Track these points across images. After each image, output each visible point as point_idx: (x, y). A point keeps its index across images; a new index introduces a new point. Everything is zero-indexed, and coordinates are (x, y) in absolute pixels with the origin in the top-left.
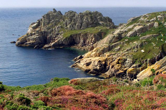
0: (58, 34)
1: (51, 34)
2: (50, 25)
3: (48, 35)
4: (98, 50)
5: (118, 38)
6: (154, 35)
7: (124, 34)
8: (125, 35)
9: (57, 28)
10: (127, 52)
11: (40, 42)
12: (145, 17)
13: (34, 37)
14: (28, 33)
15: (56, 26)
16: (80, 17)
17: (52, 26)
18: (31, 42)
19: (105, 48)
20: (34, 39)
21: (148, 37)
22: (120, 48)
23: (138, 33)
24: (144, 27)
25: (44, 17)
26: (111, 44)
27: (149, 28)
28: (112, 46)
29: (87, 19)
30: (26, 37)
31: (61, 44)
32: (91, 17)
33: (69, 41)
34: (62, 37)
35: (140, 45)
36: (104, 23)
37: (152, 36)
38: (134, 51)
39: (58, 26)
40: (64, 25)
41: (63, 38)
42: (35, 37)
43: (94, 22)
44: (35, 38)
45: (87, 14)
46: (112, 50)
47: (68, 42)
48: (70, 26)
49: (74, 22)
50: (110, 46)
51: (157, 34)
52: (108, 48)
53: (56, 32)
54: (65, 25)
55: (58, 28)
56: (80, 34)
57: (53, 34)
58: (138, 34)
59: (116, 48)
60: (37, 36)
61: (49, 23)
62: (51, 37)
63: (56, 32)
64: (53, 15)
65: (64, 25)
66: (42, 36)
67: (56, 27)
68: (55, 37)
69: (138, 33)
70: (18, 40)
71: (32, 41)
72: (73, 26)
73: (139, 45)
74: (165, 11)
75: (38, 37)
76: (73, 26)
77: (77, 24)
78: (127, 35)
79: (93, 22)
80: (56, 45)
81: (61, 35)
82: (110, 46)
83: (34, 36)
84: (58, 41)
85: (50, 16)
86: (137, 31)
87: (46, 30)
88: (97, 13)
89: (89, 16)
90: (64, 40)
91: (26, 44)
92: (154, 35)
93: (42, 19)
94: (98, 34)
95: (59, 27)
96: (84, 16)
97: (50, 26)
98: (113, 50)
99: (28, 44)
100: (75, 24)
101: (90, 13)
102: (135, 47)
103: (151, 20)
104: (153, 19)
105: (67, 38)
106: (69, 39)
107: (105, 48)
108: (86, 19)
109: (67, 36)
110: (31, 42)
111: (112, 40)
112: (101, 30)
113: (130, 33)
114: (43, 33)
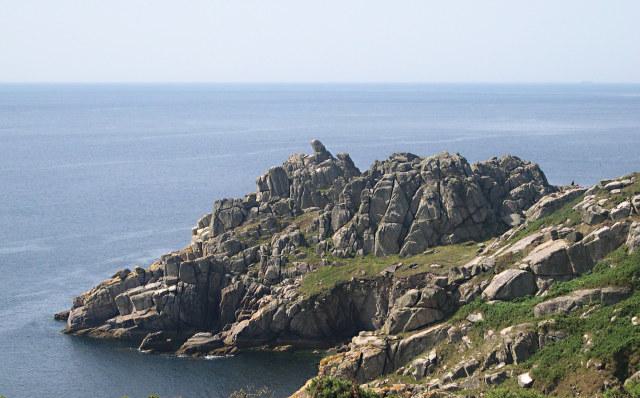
0: (277, 279)
1: (247, 277)
2: (245, 230)
3: (230, 279)
4: (330, 367)
5: (439, 308)
6: (605, 290)
7: (471, 287)
8: (476, 288)
9: (276, 245)
10: (454, 385)
11: (182, 315)
12: (604, 189)
13: (156, 288)
14: (128, 272)
15: (276, 235)
16: (401, 186)
17: (258, 235)
18: (136, 314)
19: (365, 356)
20: (147, 302)
21: (574, 304)
22: (435, 360)
23: (543, 282)
24: (574, 250)
25: (262, 184)
26: (400, 338)
27: (598, 251)
28: (405, 348)
29: (436, 198)
30: (112, 291)
31: (281, 331)
32: (459, 191)
33: (324, 318)
34: (289, 294)
35: (520, 344)
37: (596, 296)
38: (488, 380)
39: (283, 237)
40: (315, 229)
41: (294, 299)
42: (156, 292)
43: (475, 217)
44: (158, 297)
45: (438, 174)
46: (402, 372)
48: (346, 237)
49: (365, 217)
50: (393, 347)
51: (624, 290)
52: (381, 359)
53: (270, 268)
54: (322, 230)
55: (282, 244)
57: (256, 275)
58: (540, 282)
59: (420, 360)
60: (170, 283)
62: (242, 289)
63: (270, 268)
64: (308, 176)
65: (315, 229)
66: (192, 286)
67: (277, 238)
68: (260, 295)
69: (543, 282)
70: (78, 304)
71: (139, 313)
72: (359, 237)
73: (517, 341)
75: (175, 292)
76: (359, 237)
77: (381, 226)
78: (488, 288)
79: (470, 216)
80: (256, 336)
81: (292, 282)
82: (393, 347)
83: (153, 285)
84: (268, 315)
85: (291, 182)
86: (535, 269)
87: (221, 256)
88: (513, 162)
89: (445, 183)
90: (298, 307)
91: (114, 325)
92: (606, 294)
95: (287, 239)
96: (421, 181)
97: (248, 235)
98: (406, 371)
99: (120, 325)
100: (372, 225)
101: (459, 167)
102: (499, 356)
103: (614, 211)
104: (624, 204)
105: (314, 298)
106: (323, 305)
107: (365, 356)
108: (429, 200)
109: (315, 289)
110: (134, 318)
111: (408, 314)
113: (504, 277)
114: (204, 270)
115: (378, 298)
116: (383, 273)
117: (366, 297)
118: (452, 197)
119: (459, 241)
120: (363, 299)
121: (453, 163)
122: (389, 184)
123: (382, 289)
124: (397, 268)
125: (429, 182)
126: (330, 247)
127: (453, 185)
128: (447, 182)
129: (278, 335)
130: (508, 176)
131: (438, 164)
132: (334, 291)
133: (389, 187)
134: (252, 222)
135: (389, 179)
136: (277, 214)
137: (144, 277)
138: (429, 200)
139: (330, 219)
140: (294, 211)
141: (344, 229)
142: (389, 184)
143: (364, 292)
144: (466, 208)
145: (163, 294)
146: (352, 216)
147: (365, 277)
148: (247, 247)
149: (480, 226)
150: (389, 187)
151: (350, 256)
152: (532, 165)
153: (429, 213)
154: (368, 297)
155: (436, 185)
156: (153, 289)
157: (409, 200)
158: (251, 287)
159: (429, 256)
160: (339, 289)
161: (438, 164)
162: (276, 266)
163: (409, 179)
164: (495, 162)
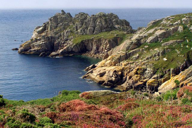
0: (67, 40)
1: (59, 40)
2: (58, 29)
3: (56, 40)
4: (113, 58)
5: (137, 45)
6: (178, 40)
7: (144, 40)
8: (145, 41)
9: (65, 32)
10: (147, 61)
11: (46, 49)
12: (168, 19)
13: (40, 43)
14: (33, 39)
15: (64, 31)
16: (93, 19)
17: (61, 31)
18: (36, 48)
19: (121, 55)
20: (39, 45)
21: (171, 43)
22: (138, 56)
23: (160, 39)
24: (167, 32)
25: (51, 20)
26: (129, 52)
27: (172, 32)
28: (130, 54)
29: (101, 22)
30: (30, 44)
31: (70, 51)
32: (106, 20)
33: (79, 48)
34: (71, 43)
35: (162, 52)
36: (120, 27)
37: (176, 42)
38: (156, 60)
39: (67, 31)
40: (74, 29)
41: (73, 44)
42: (40, 43)
43: (109, 26)
44: (41, 44)
45: (100, 17)
46: (130, 59)
47: (78, 49)
48: (81, 31)
49: (85, 26)
50: (128, 53)
51: (182, 40)
52: (125, 56)
53: (65, 38)
54: (75, 29)
55: (67, 32)
56: (92, 40)
57: (61, 39)
58: (159, 39)
59: (134, 56)
60: (43, 41)
61: (57, 27)
62: (59, 43)
63: (65, 38)
64: (62, 18)
65: (74, 29)
66: (48, 42)
67: (65, 31)
68: (64, 43)
69: (160, 39)
70: (21, 46)
71: (37, 48)
72: (84, 31)
73: (161, 52)
74: (191, 13)
75: (44, 43)
76: (84, 31)
77: (89, 28)
78: (147, 41)
79: (108, 26)
80: (65, 53)
81: (70, 41)
82: (128, 53)
83: (39, 42)
84: (68, 48)
85: (58, 19)
86: (158, 36)
87: (53, 35)
88: (112, 15)
89: (102, 19)
90: (74, 46)
91: (31, 51)
92: (179, 41)
93: (48, 22)
94: (113, 40)
95: (68, 31)
96: (97, 18)
97: (58, 30)
98: (131, 59)
99: (32, 51)
100: (87, 28)
101: (104, 15)
102: (156, 55)
103: (174, 24)
104: (177, 22)
105: (77, 44)
106: (79, 45)
107: (121, 55)
108: (99, 22)
109: (77, 42)
110: (36, 49)
111: (130, 46)
112: (117, 35)
113: (151, 38)
114: (50, 38)
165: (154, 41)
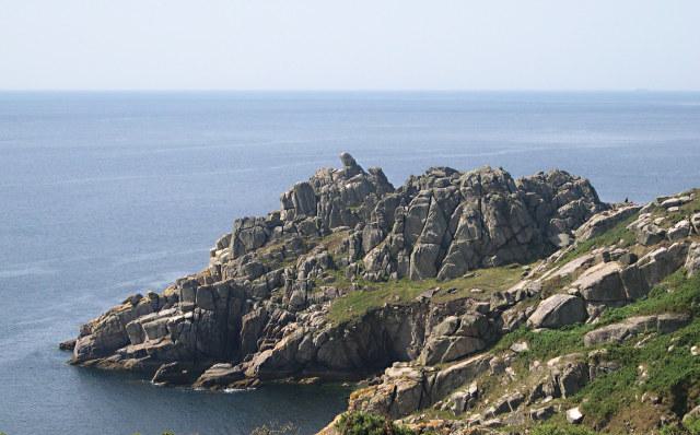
0: (303, 305)
1: (270, 303)
2: (268, 251)
3: (251, 305)
4: (361, 401)
5: (480, 337)
6: (662, 317)
7: (516, 314)
8: (521, 315)
9: (302, 268)
10: (496, 420)
11: (199, 344)
12: (660, 207)
13: (170, 315)
14: (140, 297)
15: (302, 257)
16: (439, 203)
17: (282, 256)
18: (149, 344)
19: (400, 389)
20: (161, 331)
21: (628, 332)
22: (475, 394)
23: (594, 308)
24: (628, 273)
25: (286, 201)
26: (437, 370)
27: (654, 275)
28: (442, 380)
29: (477, 216)
30: (123, 318)
31: (307, 362)
32: (502, 208)
33: (354, 347)
34: (316, 322)
35: (568, 376)
37: (652, 323)
38: (534, 415)
39: (309, 259)
40: (344, 250)
41: (321, 327)
42: (171, 320)
43: (520, 238)
44: (173, 324)
45: (479, 190)
46: (440, 406)
48: (379, 259)
49: (399, 237)
50: (430, 379)
51: (683, 317)
52: (417, 393)
53: (295, 293)
54: (352, 251)
55: (308, 267)
57: (280, 301)
58: (591, 308)
59: (459, 394)
60: (185, 310)
62: (265, 316)
63: (295, 293)
64: (336, 192)
65: (344, 250)
66: (210, 313)
67: (303, 260)
68: (285, 322)
69: (594, 308)
70: (85, 332)
71: (152, 342)
72: (392, 259)
73: (566, 373)
75: (191, 319)
76: (392, 259)
77: (417, 247)
78: (534, 315)
79: (514, 236)
80: (280, 367)
81: (319, 308)
82: (430, 379)
83: (167, 312)
84: (293, 344)
85: (318, 199)
86: (585, 294)
87: (242, 280)
88: (561, 178)
89: (487, 200)
90: (326, 335)
91: (125, 356)
92: (663, 322)
95: (314, 261)
96: (461, 198)
97: (271, 257)
98: (444, 406)
99: (131, 356)
100: (407, 246)
101: (502, 183)
102: (545, 389)
103: (671, 230)
104: (683, 223)
105: (343, 326)
106: (353, 333)
107: (400, 389)
108: (469, 219)
109: (344, 316)
110: (147, 348)
111: (446, 343)
113: (551, 303)
114: (224, 295)
115: (414, 325)
116: (419, 298)
117: (401, 325)
118: (495, 215)
119: (502, 263)
120: (397, 326)
121: (495, 178)
122: (425, 202)
123: (418, 316)
124: (435, 292)
125: (469, 199)
126: (361, 270)
127: (496, 202)
128: (489, 198)
129: (304, 366)
130: (556, 192)
131: (479, 179)
132: (365, 318)
133: (425, 205)
134: (276, 243)
135: (426, 196)
136: (303, 234)
137: (158, 303)
138: (469, 219)
139: (361, 240)
140: (322, 230)
141: (376, 250)
142: (425, 202)
143: (398, 319)
144: (510, 227)
145: (178, 321)
146: (385, 236)
147: (400, 303)
148: (270, 270)
149: (525, 247)
150: (425, 205)
151: (383, 279)
152: (582, 181)
153: (469, 232)
154: (403, 325)
155: (477, 202)
156: (167, 315)
157: (448, 219)
158: (275, 313)
159: (470, 280)
160: (371, 315)
161: (479, 179)
162: (302, 291)
163: (447, 196)
164: (542, 177)
165: (671, 307)
